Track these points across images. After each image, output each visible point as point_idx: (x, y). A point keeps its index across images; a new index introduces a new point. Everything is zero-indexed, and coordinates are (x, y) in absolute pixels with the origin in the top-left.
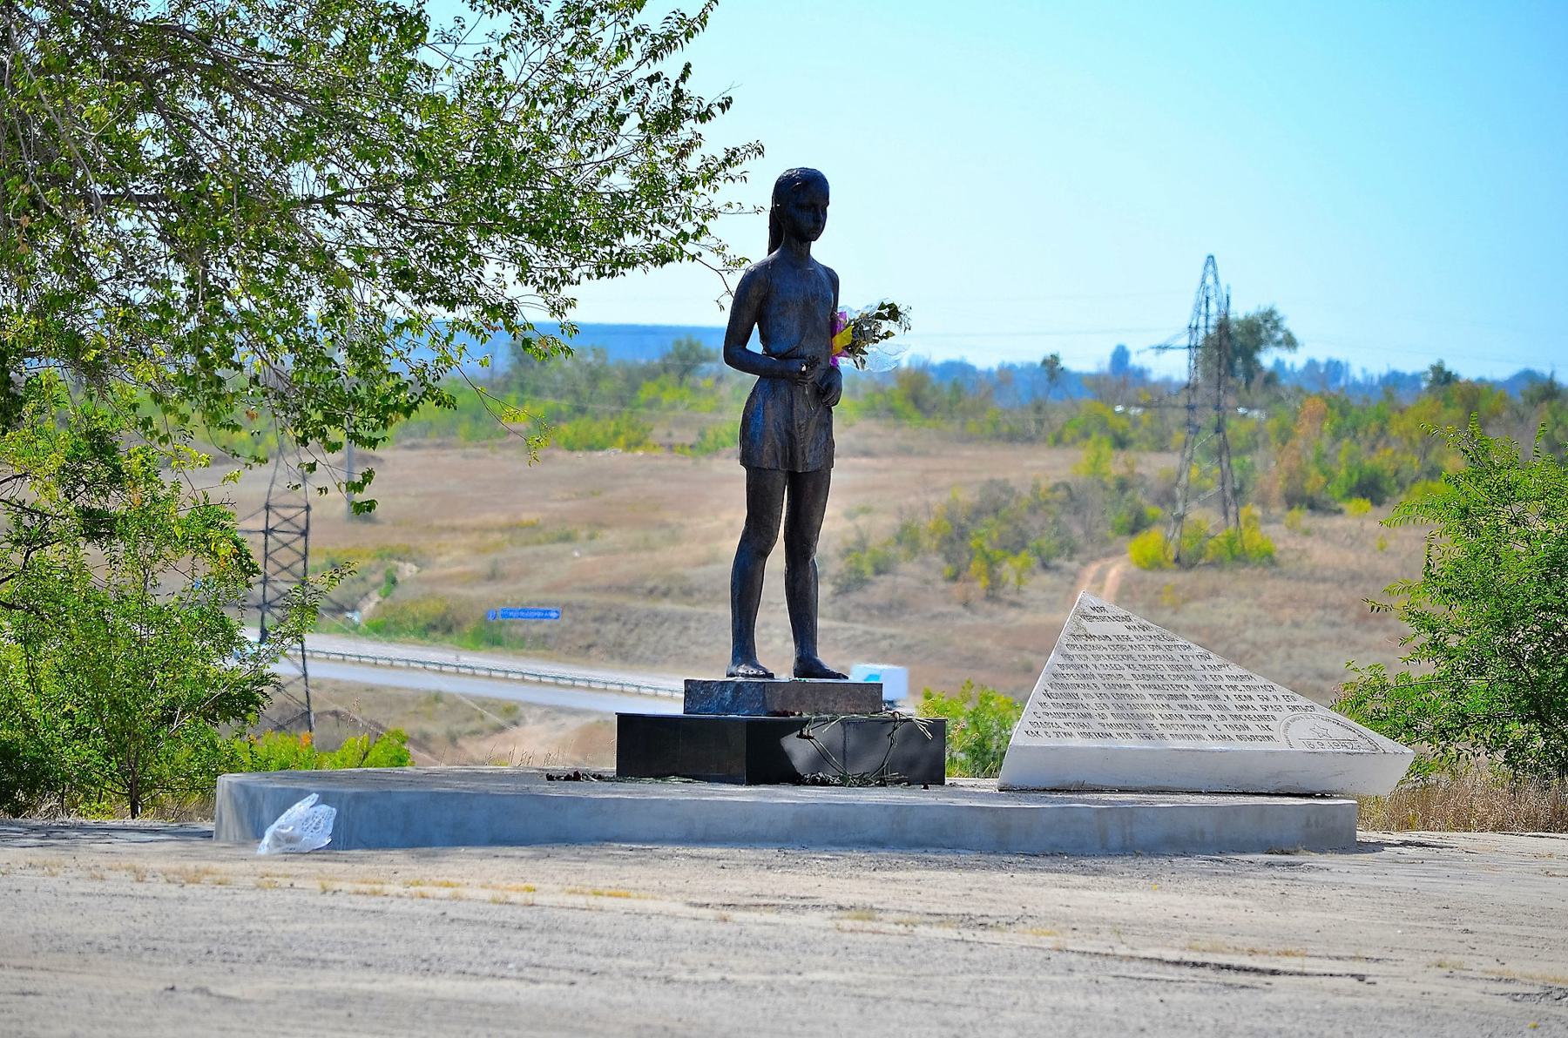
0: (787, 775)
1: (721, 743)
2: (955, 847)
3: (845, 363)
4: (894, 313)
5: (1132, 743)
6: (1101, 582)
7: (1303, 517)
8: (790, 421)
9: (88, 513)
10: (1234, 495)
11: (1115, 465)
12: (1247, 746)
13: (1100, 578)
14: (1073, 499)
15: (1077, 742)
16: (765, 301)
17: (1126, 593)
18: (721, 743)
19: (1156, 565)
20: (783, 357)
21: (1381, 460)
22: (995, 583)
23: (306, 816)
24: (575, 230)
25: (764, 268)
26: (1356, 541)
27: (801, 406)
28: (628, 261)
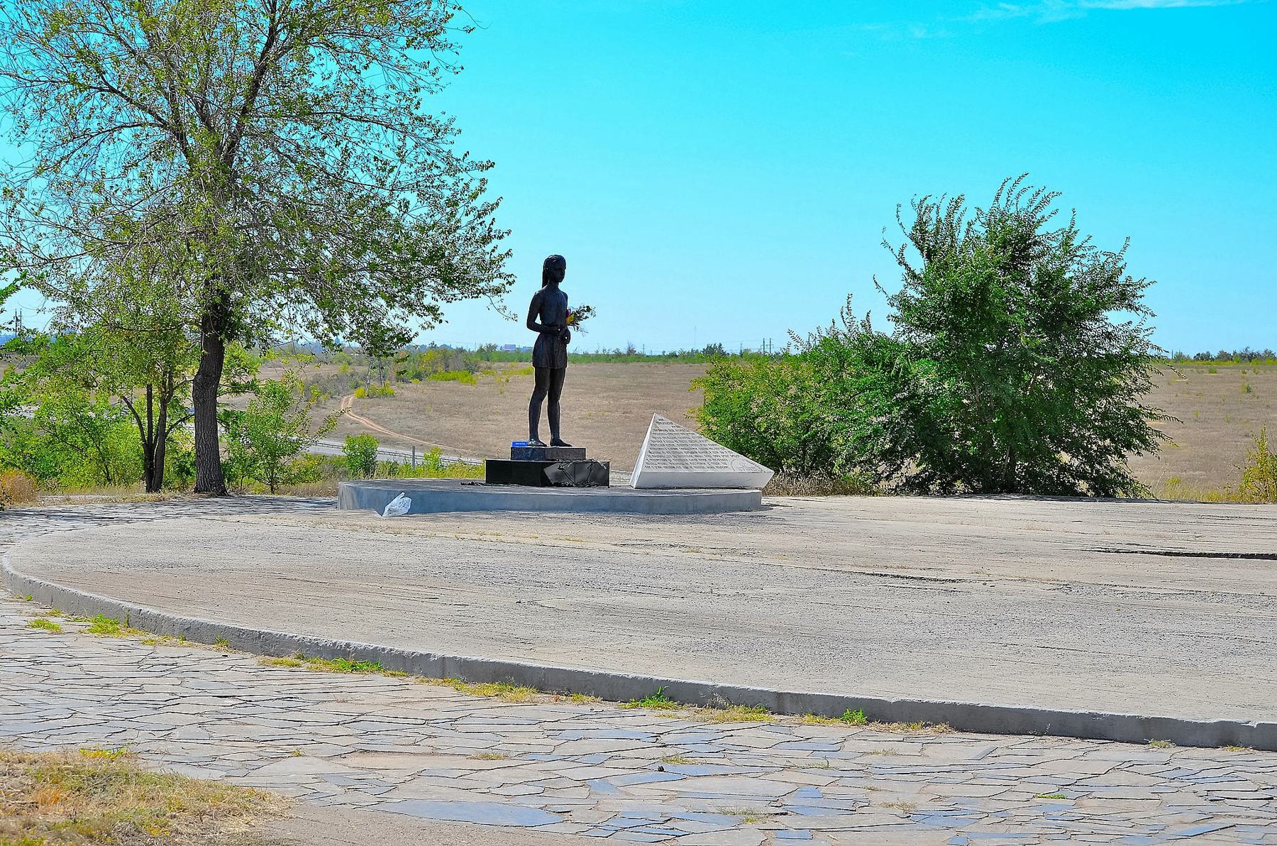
0: (545, 482)
1: (522, 471)
2: (634, 511)
3: (571, 328)
4: (589, 309)
5: (683, 470)
6: (348, 401)
7: (401, 384)
8: (552, 349)
9: (234, 384)
10: (383, 378)
11: (349, 370)
12: (719, 470)
13: (347, 400)
14: (339, 379)
15: (664, 470)
16: (543, 304)
17: (354, 404)
18: (522, 471)
19: (362, 397)
20: (550, 326)
21: (421, 368)
22: (319, 402)
23: (400, 503)
24: (455, 279)
25: (541, 292)
26: (416, 390)
27: (556, 344)
28: (479, 292)
